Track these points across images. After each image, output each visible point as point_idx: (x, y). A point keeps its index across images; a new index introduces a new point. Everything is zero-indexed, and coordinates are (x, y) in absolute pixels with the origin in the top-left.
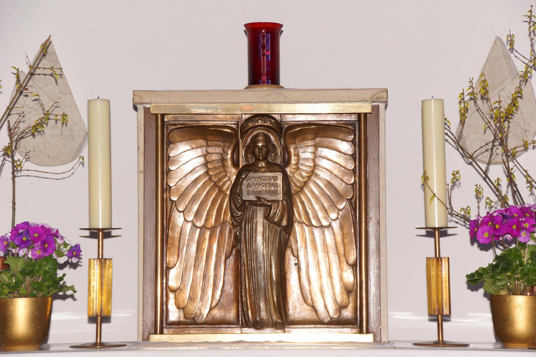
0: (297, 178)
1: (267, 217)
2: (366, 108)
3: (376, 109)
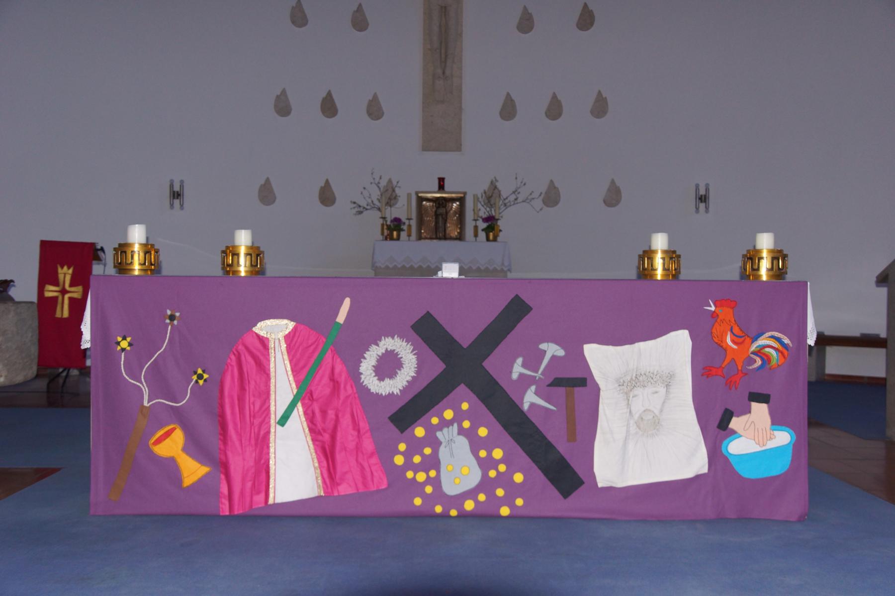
0: (448, 210)
1: (442, 218)
2: (462, 195)
3: (464, 196)
